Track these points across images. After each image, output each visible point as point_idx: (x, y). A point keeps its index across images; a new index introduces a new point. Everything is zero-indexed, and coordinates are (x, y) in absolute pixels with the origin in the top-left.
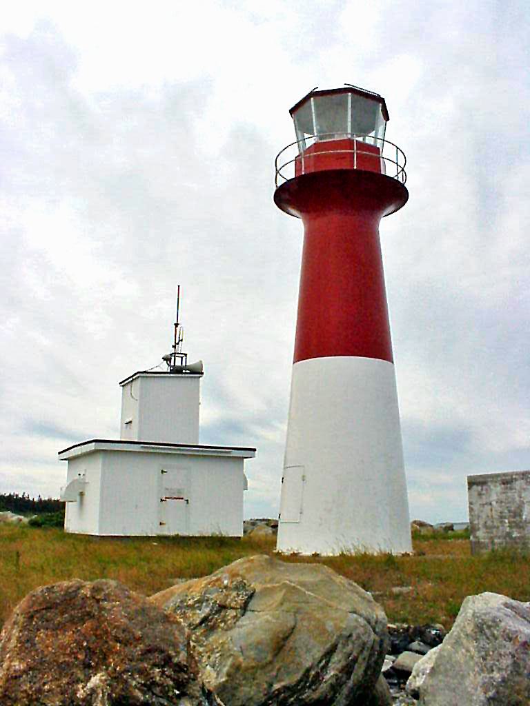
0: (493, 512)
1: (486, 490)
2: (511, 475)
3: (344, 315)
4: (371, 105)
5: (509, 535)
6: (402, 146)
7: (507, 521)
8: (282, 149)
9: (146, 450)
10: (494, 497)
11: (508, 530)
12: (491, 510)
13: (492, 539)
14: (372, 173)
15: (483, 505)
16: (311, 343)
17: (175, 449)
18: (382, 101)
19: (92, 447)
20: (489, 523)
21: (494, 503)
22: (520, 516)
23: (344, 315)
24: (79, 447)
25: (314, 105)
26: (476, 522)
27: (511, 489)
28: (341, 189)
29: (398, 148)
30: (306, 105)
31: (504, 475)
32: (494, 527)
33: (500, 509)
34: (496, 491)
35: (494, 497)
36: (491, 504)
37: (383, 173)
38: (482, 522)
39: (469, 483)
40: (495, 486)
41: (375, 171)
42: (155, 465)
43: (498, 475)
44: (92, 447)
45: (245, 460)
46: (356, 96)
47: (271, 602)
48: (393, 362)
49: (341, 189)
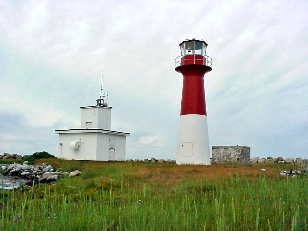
0: (221, 155)
1: (219, 150)
2: (227, 147)
3: (194, 102)
4: (200, 44)
5: (226, 161)
6: (210, 55)
7: (225, 158)
8: (176, 55)
9: (108, 133)
10: (221, 152)
11: (226, 160)
12: (220, 155)
13: (220, 162)
14: (201, 65)
15: (218, 154)
16: (186, 109)
17: (115, 133)
18: (204, 42)
19: (97, 131)
20: (219, 158)
21: (221, 153)
22: (230, 156)
23: (194, 102)
24: (84, 130)
25: (188, 44)
26: (215, 158)
27: (227, 150)
28: (194, 69)
29: (207, 56)
30: (183, 44)
31: (225, 146)
32: (221, 159)
33: (223, 155)
34: (222, 151)
35: (221, 152)
36: (220, 153)
37: (207, 65)
38: (217, 158)
39: (212, 148)
40: (222, 149)
41: (202, 64)
42: (108, 137)
43: (223, 146)
44: (97, 131)
45: (126, 137)
46: (196, 42)
47: (8, 184)
48: (206, 115)
49: (194, 69)
